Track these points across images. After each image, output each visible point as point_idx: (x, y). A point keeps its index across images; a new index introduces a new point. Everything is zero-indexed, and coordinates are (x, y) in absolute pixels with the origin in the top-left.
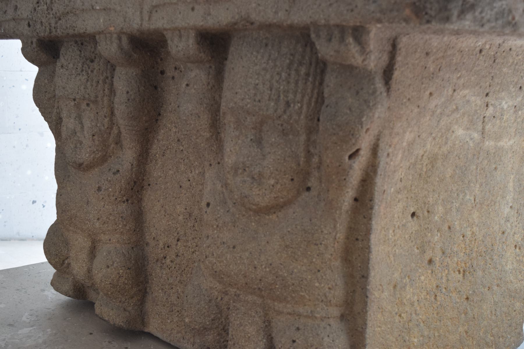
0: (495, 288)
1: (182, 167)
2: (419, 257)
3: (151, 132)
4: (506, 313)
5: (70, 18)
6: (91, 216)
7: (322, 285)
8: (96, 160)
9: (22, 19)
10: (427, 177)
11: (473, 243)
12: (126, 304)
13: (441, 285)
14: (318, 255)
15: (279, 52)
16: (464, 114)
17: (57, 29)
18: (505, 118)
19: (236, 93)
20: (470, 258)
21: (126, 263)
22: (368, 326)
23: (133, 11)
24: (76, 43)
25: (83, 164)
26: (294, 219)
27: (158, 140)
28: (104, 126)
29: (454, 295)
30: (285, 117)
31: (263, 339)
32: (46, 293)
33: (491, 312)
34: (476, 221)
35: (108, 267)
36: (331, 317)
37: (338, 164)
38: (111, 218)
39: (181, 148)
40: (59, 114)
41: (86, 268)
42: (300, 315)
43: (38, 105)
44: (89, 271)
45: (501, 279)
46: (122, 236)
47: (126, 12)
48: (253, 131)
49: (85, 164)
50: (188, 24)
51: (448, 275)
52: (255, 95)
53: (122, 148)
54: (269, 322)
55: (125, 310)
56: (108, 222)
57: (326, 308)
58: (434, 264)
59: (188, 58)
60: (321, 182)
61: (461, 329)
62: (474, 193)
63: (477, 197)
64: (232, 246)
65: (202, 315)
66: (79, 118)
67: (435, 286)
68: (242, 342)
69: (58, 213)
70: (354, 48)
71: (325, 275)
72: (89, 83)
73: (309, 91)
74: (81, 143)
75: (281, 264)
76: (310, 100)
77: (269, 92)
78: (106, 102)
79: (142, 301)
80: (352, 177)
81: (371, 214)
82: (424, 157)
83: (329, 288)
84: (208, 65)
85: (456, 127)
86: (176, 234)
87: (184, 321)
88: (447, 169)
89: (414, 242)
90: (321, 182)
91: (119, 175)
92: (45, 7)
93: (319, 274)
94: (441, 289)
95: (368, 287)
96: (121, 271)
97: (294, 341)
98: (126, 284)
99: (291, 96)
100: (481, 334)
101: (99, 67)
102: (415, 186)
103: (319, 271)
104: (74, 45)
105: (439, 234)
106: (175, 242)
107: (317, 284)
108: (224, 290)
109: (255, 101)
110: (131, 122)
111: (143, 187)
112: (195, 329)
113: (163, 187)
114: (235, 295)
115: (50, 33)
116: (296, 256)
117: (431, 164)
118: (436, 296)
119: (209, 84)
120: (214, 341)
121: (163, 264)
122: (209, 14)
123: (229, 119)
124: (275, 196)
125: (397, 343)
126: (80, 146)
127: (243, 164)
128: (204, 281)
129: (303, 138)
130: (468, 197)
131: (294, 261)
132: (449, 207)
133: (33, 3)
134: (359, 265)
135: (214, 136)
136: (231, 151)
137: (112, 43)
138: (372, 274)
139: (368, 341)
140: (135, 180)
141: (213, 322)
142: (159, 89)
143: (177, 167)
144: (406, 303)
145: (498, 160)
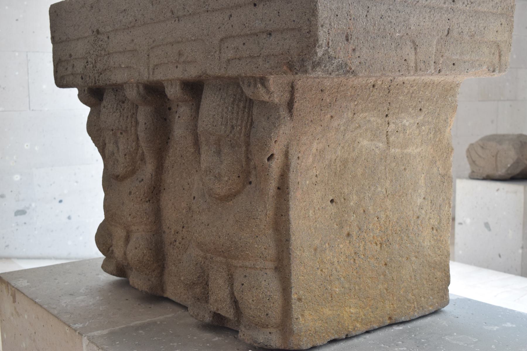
0: (414, 259)
1: (184, 175)
2: (338, 230)
3: (163, 151)
4: (426, 279)
5: (107, 73)
6: (125, 213)
7: (260, 246)
8: (127, 172)
9: (78, 74)
10: (341, 174)
11: (388, 223)
12: (150, 276)
13: (358, 252)
14: (256, 226)
15: (227, 93)
16: (366, 130)
17: (100, 80)
18: (408, 132)
19: (204, 121)
20: (386, 234)
21: (149, 245)
22: (292, 274)
23: (144, 68)
24: (113, 90)
25: (119, 176)
26: (242, 203)
27: (169, 157)
28: (132, 148)
29: (372, 261)
30: (231, 135)
31: (228, 287)
32: (100, 276)
33: (411, 277)
34: (390, 207)
35: (136, 248)
36: (267, 268)
37: (262, 165)
38: (139, 213)
39: (183, 161)
40: (104, 141)
41: (123, 252)
42: (247, 267)
43: (90, 135)
44: (125, 254)
45: (418, 252)
46: (146, 227)
47: (140, 69)
48: (215, 146)
49: (120, 175)
50: (174, 77)
51: (365, 246)
52: (213, 122)
53: (145, 164)
54: (232, 275)
55: (149, 280)
56: (136, 217)
57: (263, 262)
58: (351, 236)
59: (177, 99)
60: (257, 178)
61: (380, 286)
62: (385, 187)
63: (388, 190)
64: (207, 225)
65: (191, 274)
66: (116, 143)
67: (353, 252)
68: (216, 291)
69: (105, 214)
70: (261, 90)
71: (261, 239)
72: (121, 118)
73: (246, 118)
74: (118, 161)
75: (234, 233)
76: (246, 124)
77: (221, 120)
78: (133, 131)
79: (161, 274)
80: (272, 173)
81: (288, 198)
82: (337, 161)
83: (265, 249)
84: (191, 103)
85: (361, 139)
86: (181, 223)
87: (181, 279)
88: (357, 169)
89: (333, 220)
90: (257, 178)
91: (143, 182)
92: (92, 66)
93: (257, 239)
94: (359, 255)
95: (291, 248)
96: (145, 251)
97: (243, 284)
98: (149, 260)
99: (234, 122)
100: (401, 292)
101: (128, 106)
102: (332, 181)
103: (257, 237)
104: (112, 91)
105: (355, 216)
106: (181, 229)
107: (256, 246)
108: (204, 256)
109: (213, 126)
110: (149, 144)
111: (160, 191)
112: (188, 284)
113: (173, 190)
114: (211, 258)
115: (95, 83)
116: (243, 228)
117: (344, 166)
118: (355, 260)
119: (192, 115)
120: (201, 293)
121: (175, 245)
122: (186, 71)
123: (202, 139)
124: (229, 188)
125: (320, 290)
126: (117, 163)
127: (209, 168)
128: (193, 251)
129: (244, 148)
130: (379, 189)
131: (242, 231)
132: (362, 196)
133: (84, 63)
134: (284, 232)
135: (197, 151)
136: (204, 160)
137: (133, 90)
138: (293, 238)
139: (293, 285)
140: (154, 186)
141: (199, 278)
142: (168, 121)
143: (181, 176)
144: (326, 262)
145: (406, 163)
